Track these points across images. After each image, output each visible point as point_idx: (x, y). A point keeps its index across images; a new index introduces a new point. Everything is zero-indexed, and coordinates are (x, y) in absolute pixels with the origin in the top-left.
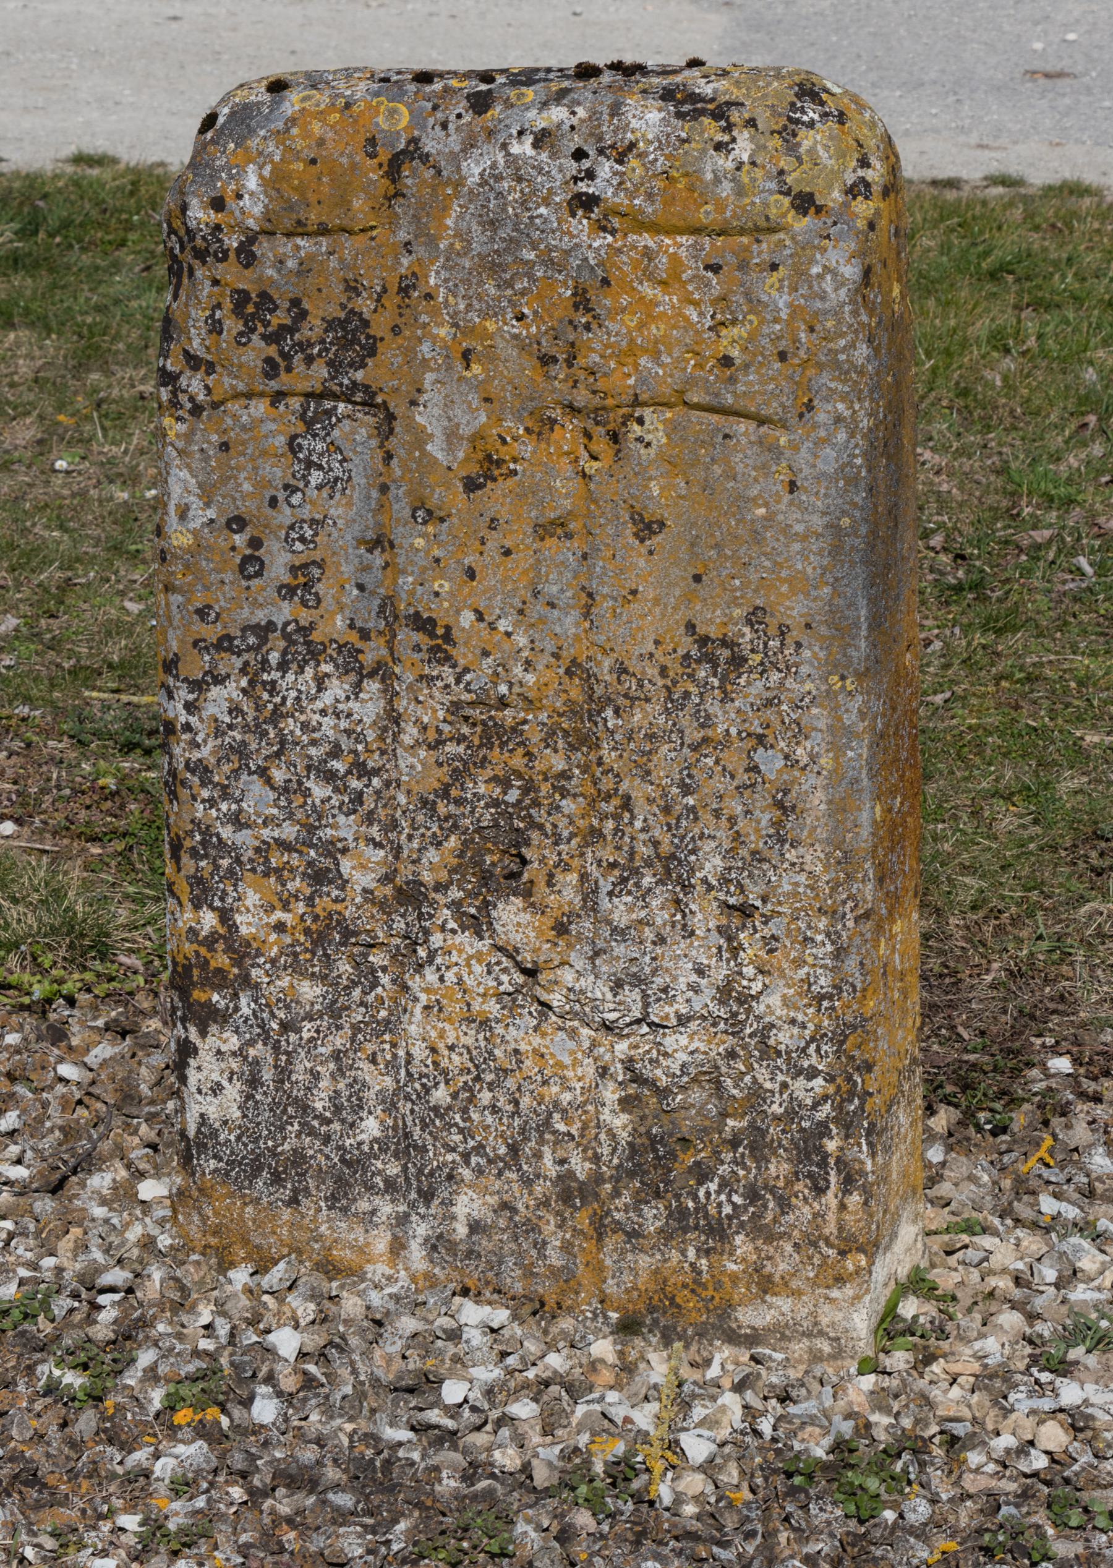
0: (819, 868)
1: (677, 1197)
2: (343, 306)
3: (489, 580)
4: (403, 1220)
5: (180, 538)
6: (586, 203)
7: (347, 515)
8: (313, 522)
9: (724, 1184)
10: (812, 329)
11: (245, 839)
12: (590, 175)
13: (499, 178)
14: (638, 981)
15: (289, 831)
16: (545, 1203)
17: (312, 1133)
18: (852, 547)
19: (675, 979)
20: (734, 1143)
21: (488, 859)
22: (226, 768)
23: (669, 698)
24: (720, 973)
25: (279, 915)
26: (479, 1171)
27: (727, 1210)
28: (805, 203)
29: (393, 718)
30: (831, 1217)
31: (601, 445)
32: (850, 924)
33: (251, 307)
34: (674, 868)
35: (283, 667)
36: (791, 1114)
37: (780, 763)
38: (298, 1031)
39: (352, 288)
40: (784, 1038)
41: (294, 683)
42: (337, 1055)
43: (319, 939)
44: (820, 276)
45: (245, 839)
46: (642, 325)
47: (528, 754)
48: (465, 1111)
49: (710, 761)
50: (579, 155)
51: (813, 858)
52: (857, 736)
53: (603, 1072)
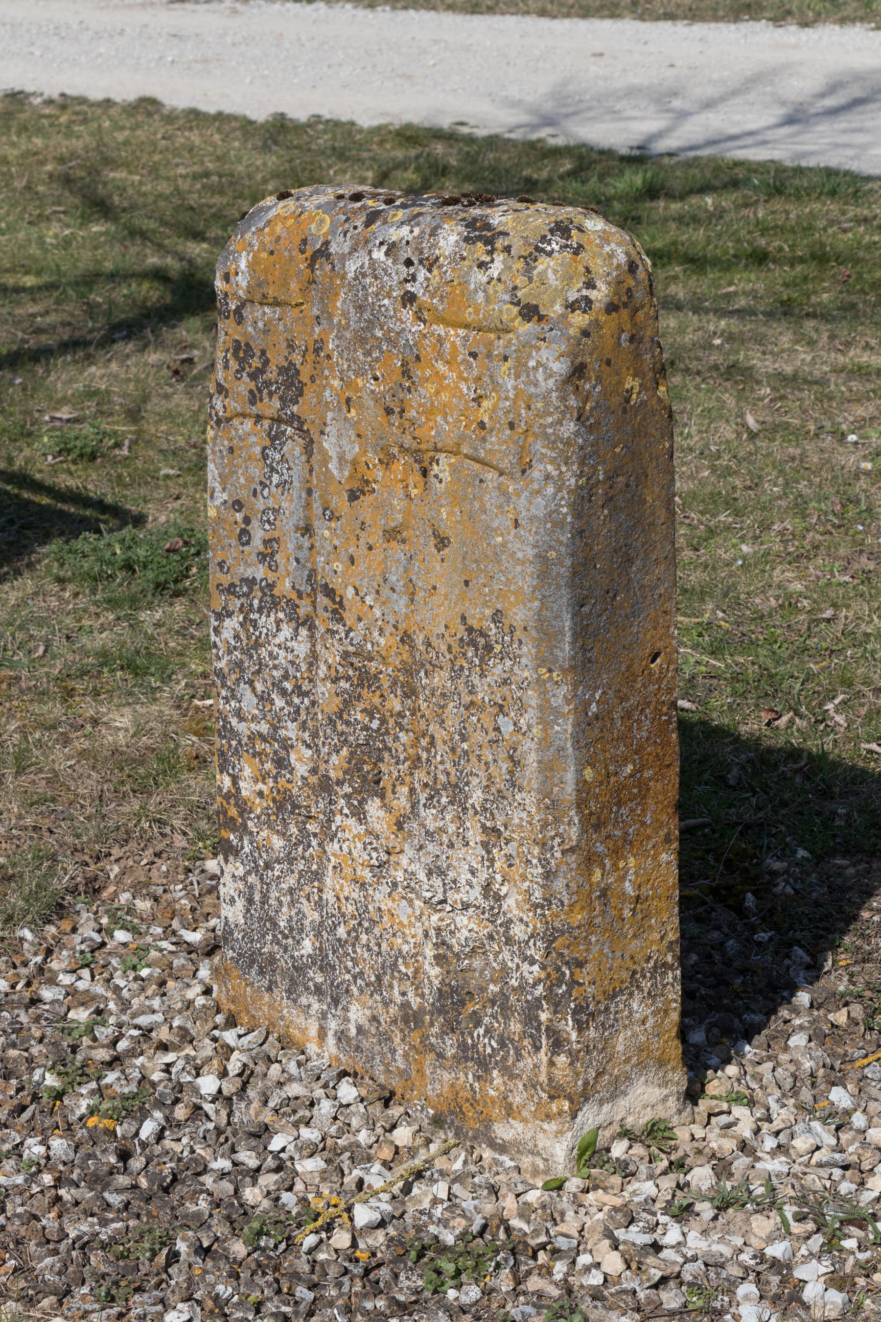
0: (534, 810)
1: (463, 1034)
2: (286, 358)
3: (361, 566)
4: (324, 1016)
6: (409, 298)
9: (487, 1031)
10: (529, 407)
12: (414, 278)
13: (364, 275)
14: (442, 873)
15: (264, 728)
18: (558, 574)
19: (459, 874)
21: (366, 768)
22: (234, 677)
23: (452, 669)
24: (483, 876)
25: (260, 786)
26: (361, 991)
27: (489, 1050)
28: (530, 312)
29: (313, 658)
30: (544, 1069)
32: (558, 855)
34: (457, 791)
37: (511, 728)
38: (273, 870)
39: (291, 346)
41: (266, 622)
42: (291, 891)
43: (280, 808)
44: (535, 369)
46: (437, 393)
47: (382, 696)
48: (354, 946)
49: (475, 719)
50: (409, 263)
51: (530, 799)
52: (563, 715)
53: (426, 935)
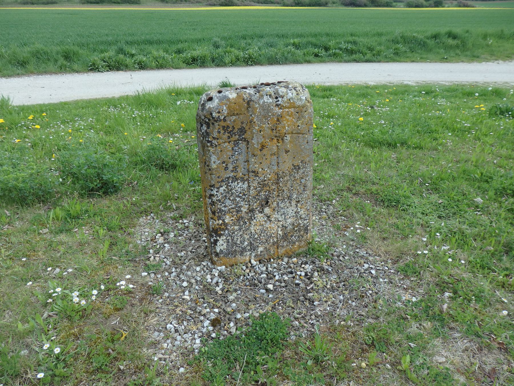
5: (214, 166)
7: (242, 158)
8: (236, 160)
11: (226, 209)
15: (233, 206)
16: (271, 246)
17: (237, 246)
20: (296, 231)
29: (249, 186)
31: (280, 141)
33: (225, 128)
34: (290, 198)
35: (232, 182)
36: (304, 225)
40: (303, 216)
41: (233, 185)
42: (241, 235)
45: (226, 209)
53: (278, 227)
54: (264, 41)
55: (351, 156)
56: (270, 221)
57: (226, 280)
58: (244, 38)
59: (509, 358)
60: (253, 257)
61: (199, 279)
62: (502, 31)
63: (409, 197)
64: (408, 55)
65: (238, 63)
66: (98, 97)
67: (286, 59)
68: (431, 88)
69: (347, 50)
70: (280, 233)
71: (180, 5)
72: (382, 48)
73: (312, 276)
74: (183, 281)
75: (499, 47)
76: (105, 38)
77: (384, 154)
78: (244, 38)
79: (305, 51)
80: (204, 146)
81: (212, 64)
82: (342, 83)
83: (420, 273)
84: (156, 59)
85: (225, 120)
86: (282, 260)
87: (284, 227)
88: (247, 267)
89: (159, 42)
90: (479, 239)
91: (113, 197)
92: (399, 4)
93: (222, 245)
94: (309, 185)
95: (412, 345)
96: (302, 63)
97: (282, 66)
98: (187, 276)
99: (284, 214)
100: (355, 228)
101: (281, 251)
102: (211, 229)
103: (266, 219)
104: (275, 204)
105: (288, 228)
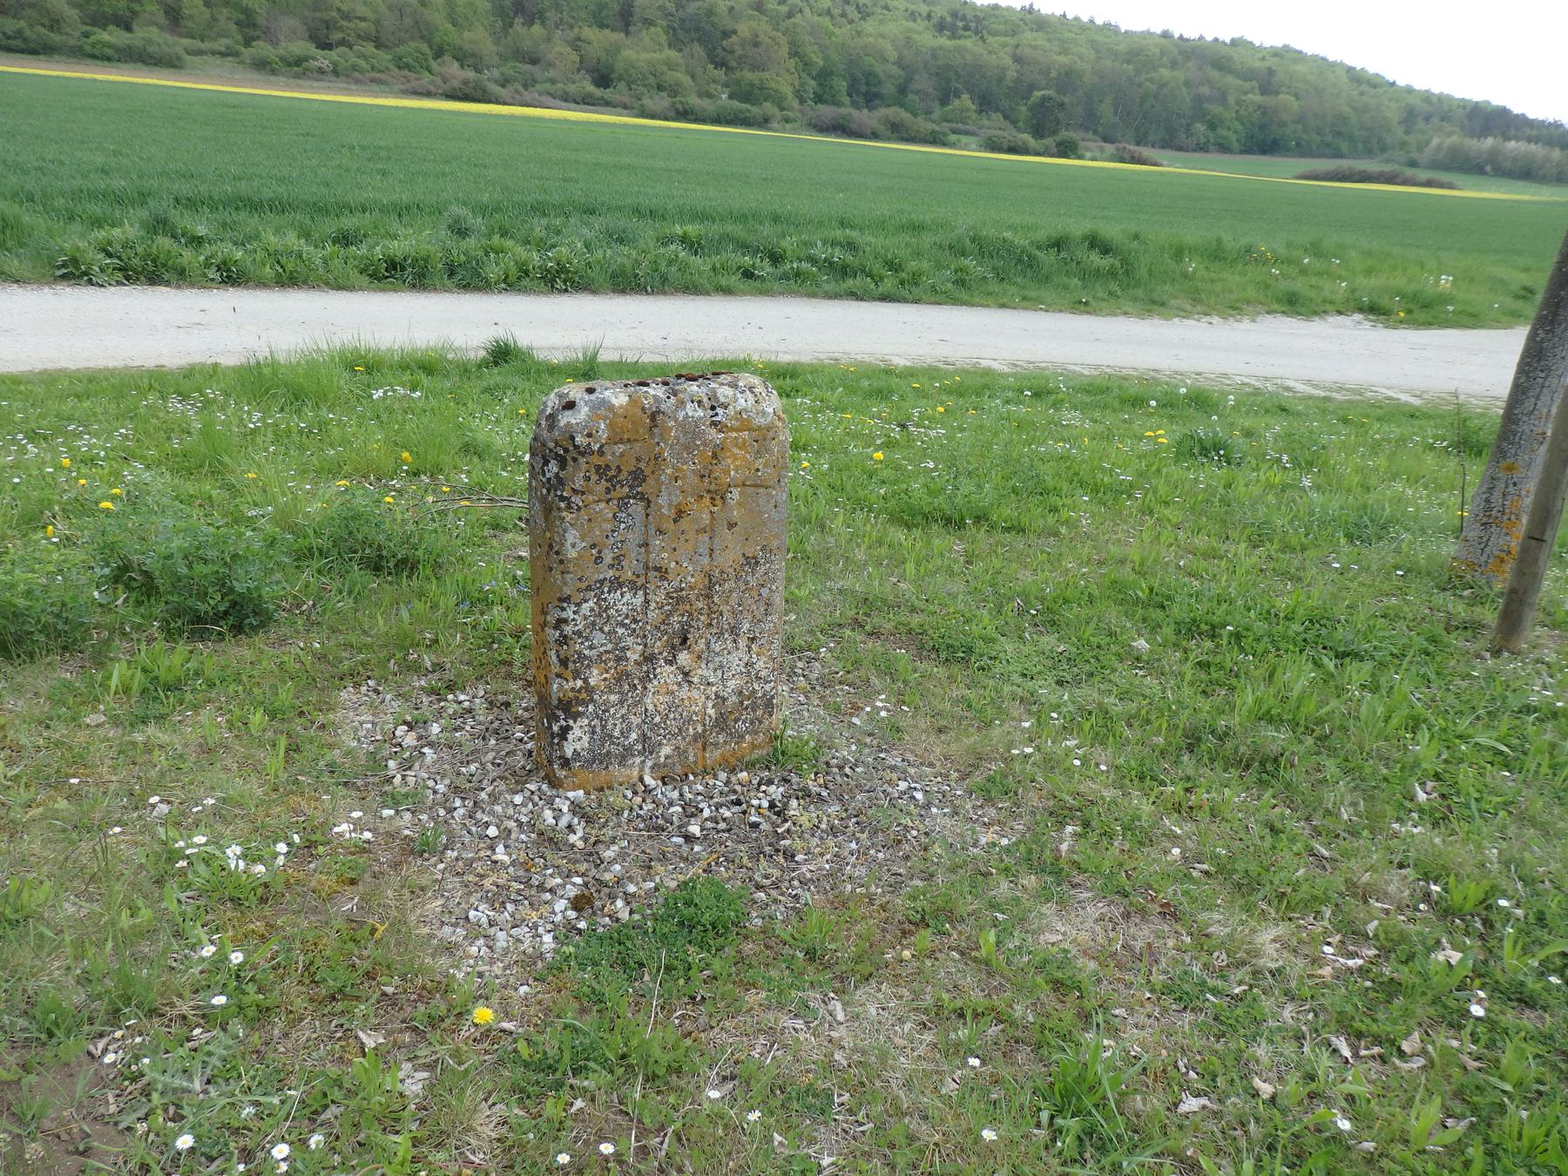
5: (572, 554)
7: (634, 537)
15: (610, 647)
29: (647, 602)
31: (718, 502)
33: (601, 471)
34: (734, 630)
40: (763, 674)
41: (612, 598)
54: (597, 222)
55: (859, 546)
56: (690, 683)
57: (589, 820)
58: (539, 209)
59: (1179, 928)
60: (647, 770)
61: (524, 819)
62: (1219, 240)
63: (993, 640)
64: (990, 288)
65: (526, 282)
66: (111, 364)
67: (664, 279)
68: (1047, 381)
69: (829, 265)
70: (711, 711)
71: (315, 84)
72: (925, 265)
73: (786, 806)
74: (487, 825)
75: (1212, 281)
76: (101, 184)
77: (937, 542)
78: (539, 209)
79: (716, 259)
80: (548, 510)
81: (448, 282)
82: (822, 356)
83: (1016, 793)
84: (275, 256)
85: (601, 452)
86: (715, 777)
87: (720, 699)
88: (635, 793)
89: (281, 207)
90: (1136, 724)
91: (259, 640)
92: (964, 139)
93: (580, 739)
94: (778, 601)
95: (1000, 916)
96: (708, 294)
97: (651, 298)
98: (492, 813)
99: (721, 667)
100: (874, 707)
101: (713, 756)
102: (555, 702)
103: (680, 678)
104: (702, 644)
105: (728, 703)
